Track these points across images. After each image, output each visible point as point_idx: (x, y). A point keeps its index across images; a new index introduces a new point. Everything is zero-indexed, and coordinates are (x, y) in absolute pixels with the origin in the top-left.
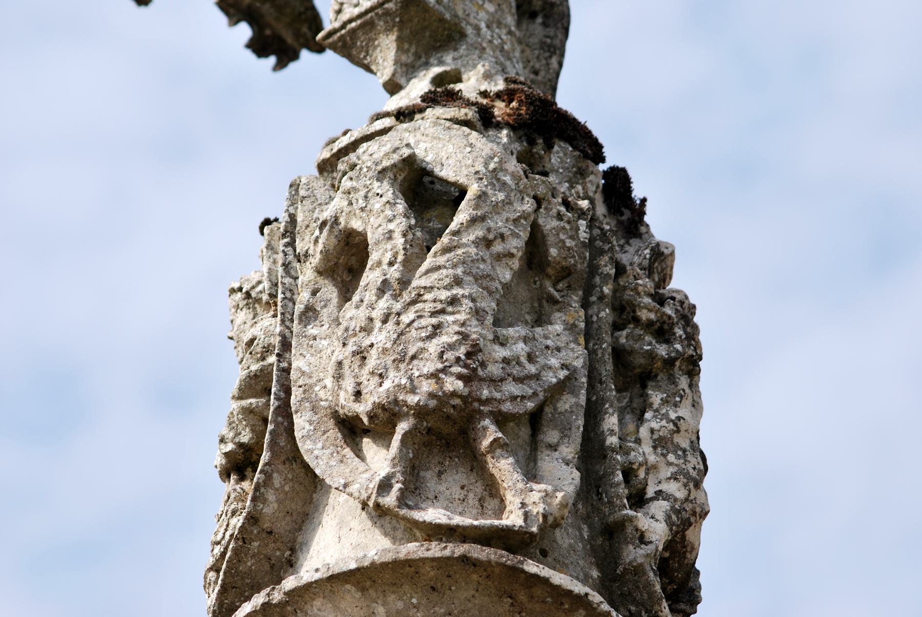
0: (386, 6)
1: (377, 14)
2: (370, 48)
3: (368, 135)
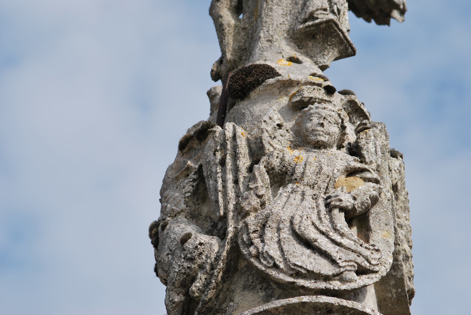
0: (350, 48)
1: (346, 45)
2: (332, 46)
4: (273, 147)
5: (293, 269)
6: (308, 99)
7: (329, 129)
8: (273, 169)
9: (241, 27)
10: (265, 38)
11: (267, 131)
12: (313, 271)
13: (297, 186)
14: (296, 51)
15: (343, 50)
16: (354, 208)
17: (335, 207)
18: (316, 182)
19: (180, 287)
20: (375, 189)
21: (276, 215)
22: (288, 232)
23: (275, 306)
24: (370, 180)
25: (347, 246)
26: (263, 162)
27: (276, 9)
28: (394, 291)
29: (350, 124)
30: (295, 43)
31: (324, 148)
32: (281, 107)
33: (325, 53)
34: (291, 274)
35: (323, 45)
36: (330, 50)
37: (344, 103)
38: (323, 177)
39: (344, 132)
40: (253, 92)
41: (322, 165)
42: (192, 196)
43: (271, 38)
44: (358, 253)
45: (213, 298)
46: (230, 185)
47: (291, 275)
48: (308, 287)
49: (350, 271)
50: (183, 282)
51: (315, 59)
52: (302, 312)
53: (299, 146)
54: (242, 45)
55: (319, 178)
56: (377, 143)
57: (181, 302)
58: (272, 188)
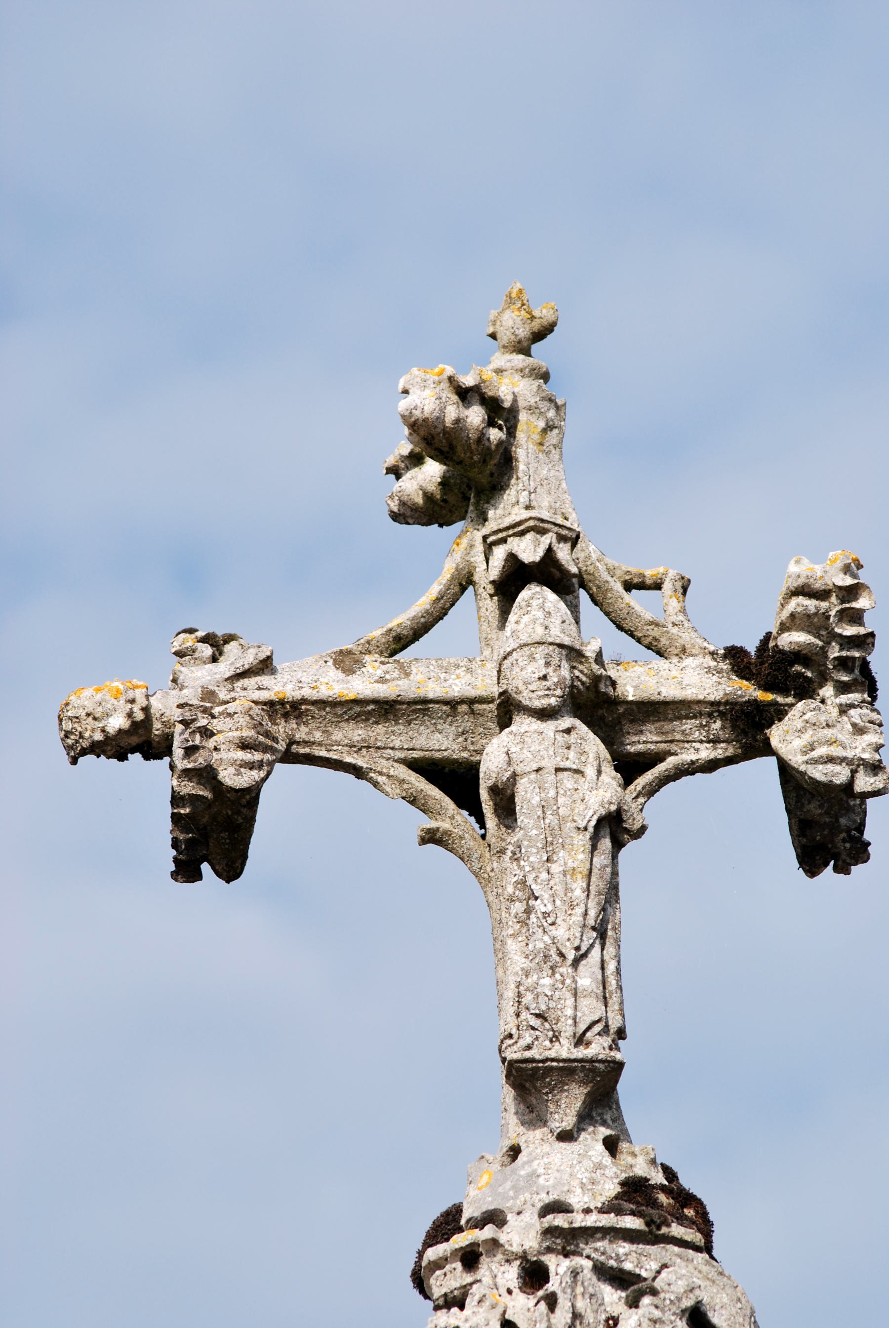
0: (597, 1065)
3: (616, 1228)
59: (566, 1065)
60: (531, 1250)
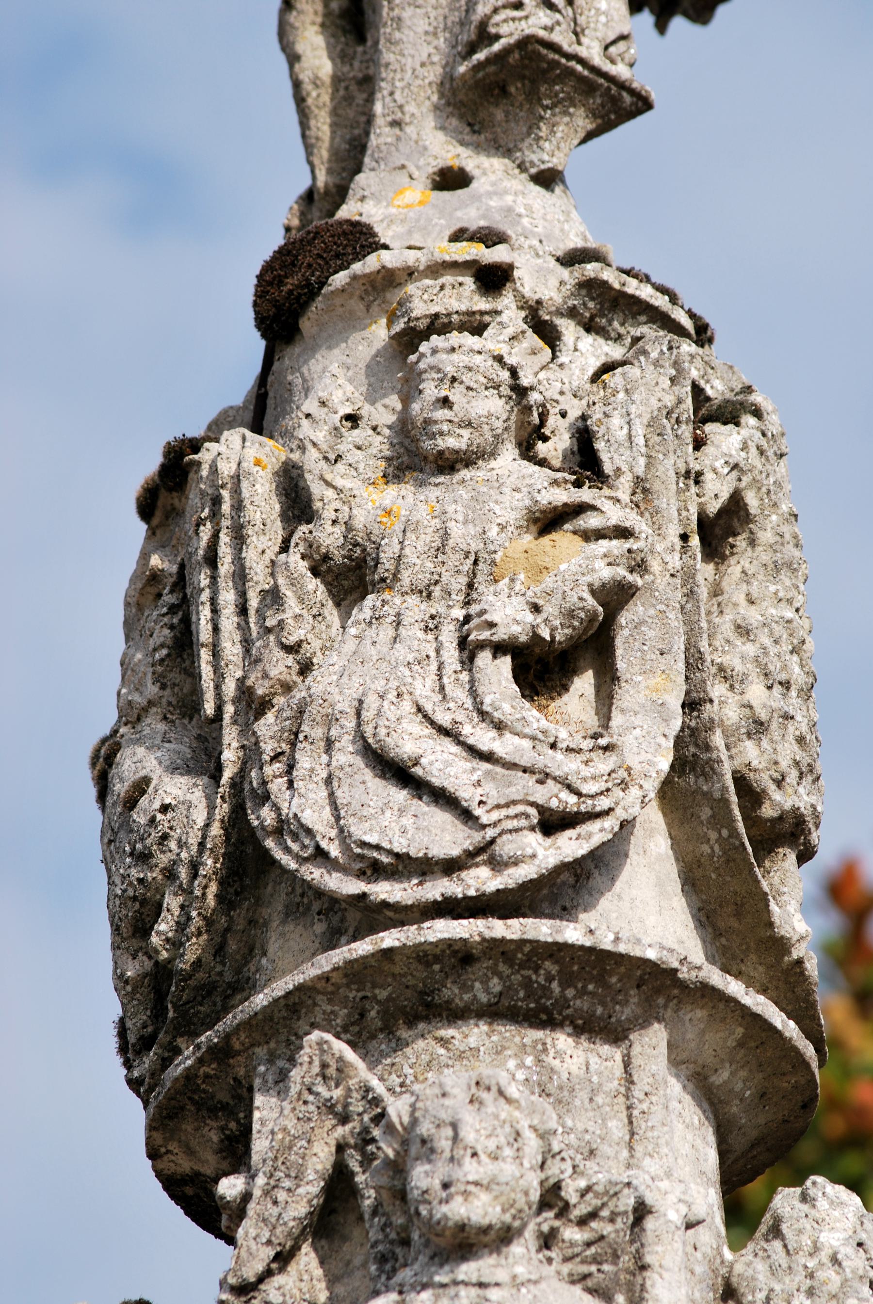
0: (625, 94)
1: (609, 89)
2: (560, 106)
4: (335, 488)
5: (361, 857)
6: (428, 320)
7: (470, 409)
8: (326, 558)
9: (354, 78)
10: (384, 116)
11: (314, 444)
12: (408, 854)
13: (383, 601)
14: (462, 143)
15: (603, 105)
16: (536, 637)
17: (481, 645)
18: (437, 577)
19: (134, 935)
20: (611, 560)
21: (321, 701)
22: (351, 749)
23: (319, 972)
24: (599, 535)
25: (508, 758)
26: (297, 545)
27: (410, 18)
28: (713, 835)
29: (610, 342)
30: (461, 117)
31: (467, 466)
32: (373, 351)
33: (541, 134)
34: (360, 870)
35: (531, 111)
36: (557, 119)
37: (569, 293)
38: (453, 559)
39: (524, 402)
40: (305, 319)
41: (449, 524)
42: (174, 656)
43: (399, 115)
44: (540, 773)
45: (208, 958)
46: (229, 621)
47: (361, 874)
48: (398, 902)
49: (517, 830)
50: (138, 921)
51: (518, 154)
52: (394, 975)
53: (409, 468)
54: (360, 135)
55: (443, 563)
56: (633, 409)
57: (145, 975)
58: (342, 608)
59: (591, 76)
60: (550, 302)
